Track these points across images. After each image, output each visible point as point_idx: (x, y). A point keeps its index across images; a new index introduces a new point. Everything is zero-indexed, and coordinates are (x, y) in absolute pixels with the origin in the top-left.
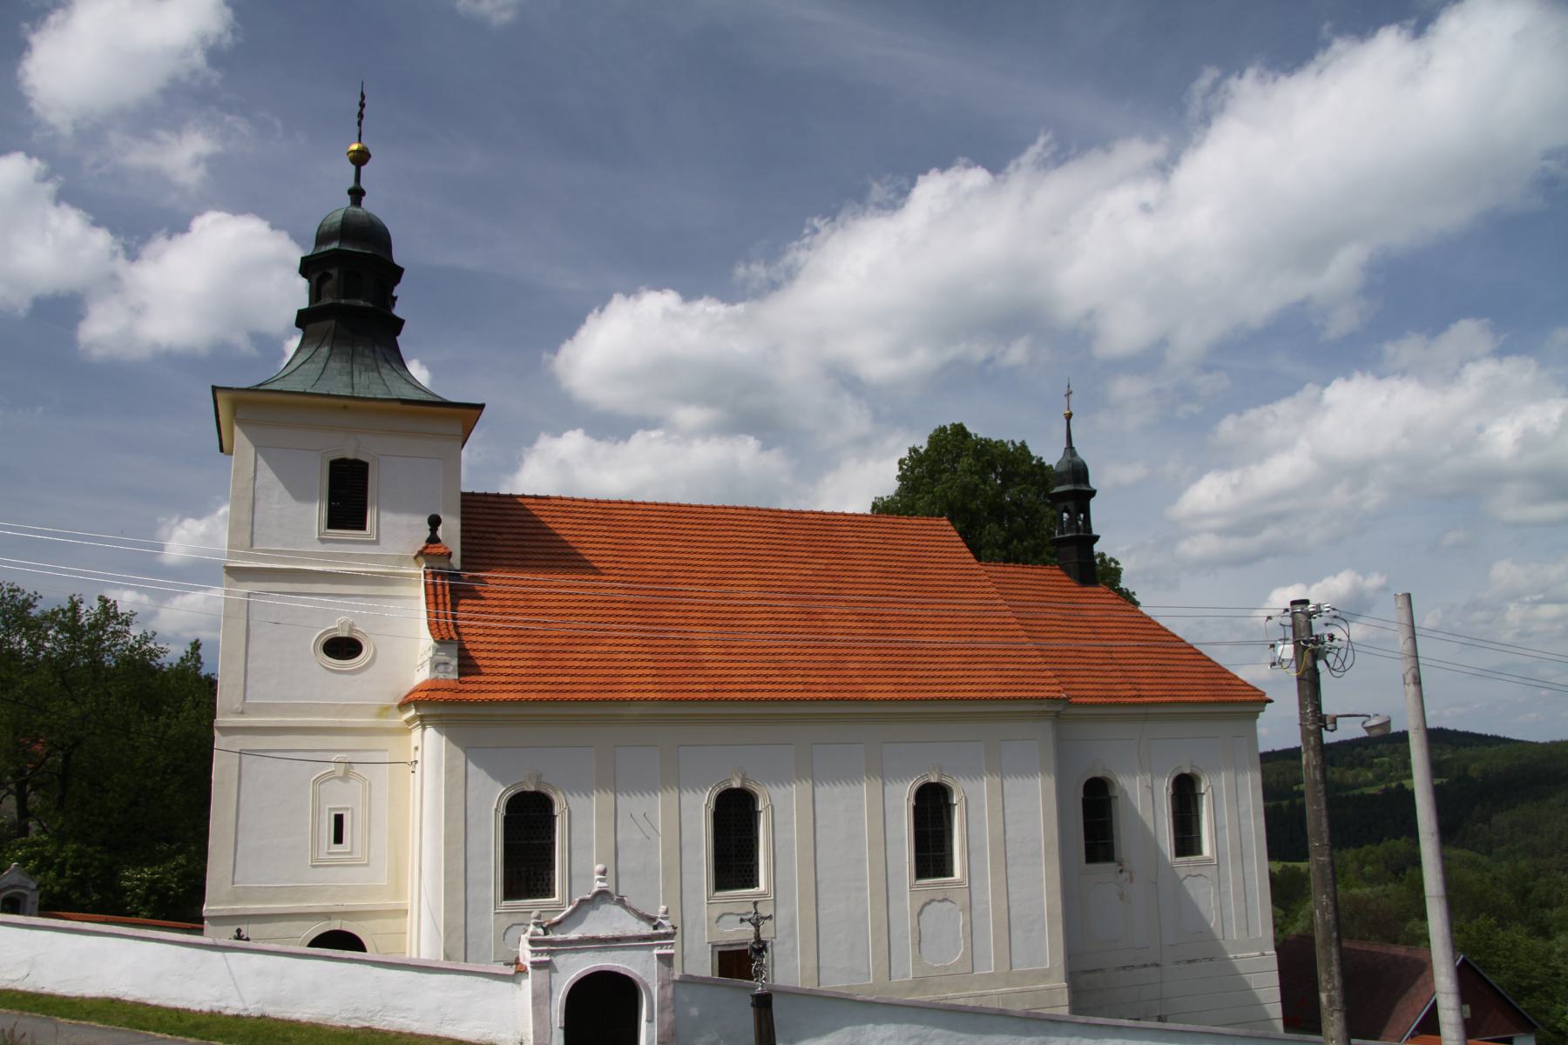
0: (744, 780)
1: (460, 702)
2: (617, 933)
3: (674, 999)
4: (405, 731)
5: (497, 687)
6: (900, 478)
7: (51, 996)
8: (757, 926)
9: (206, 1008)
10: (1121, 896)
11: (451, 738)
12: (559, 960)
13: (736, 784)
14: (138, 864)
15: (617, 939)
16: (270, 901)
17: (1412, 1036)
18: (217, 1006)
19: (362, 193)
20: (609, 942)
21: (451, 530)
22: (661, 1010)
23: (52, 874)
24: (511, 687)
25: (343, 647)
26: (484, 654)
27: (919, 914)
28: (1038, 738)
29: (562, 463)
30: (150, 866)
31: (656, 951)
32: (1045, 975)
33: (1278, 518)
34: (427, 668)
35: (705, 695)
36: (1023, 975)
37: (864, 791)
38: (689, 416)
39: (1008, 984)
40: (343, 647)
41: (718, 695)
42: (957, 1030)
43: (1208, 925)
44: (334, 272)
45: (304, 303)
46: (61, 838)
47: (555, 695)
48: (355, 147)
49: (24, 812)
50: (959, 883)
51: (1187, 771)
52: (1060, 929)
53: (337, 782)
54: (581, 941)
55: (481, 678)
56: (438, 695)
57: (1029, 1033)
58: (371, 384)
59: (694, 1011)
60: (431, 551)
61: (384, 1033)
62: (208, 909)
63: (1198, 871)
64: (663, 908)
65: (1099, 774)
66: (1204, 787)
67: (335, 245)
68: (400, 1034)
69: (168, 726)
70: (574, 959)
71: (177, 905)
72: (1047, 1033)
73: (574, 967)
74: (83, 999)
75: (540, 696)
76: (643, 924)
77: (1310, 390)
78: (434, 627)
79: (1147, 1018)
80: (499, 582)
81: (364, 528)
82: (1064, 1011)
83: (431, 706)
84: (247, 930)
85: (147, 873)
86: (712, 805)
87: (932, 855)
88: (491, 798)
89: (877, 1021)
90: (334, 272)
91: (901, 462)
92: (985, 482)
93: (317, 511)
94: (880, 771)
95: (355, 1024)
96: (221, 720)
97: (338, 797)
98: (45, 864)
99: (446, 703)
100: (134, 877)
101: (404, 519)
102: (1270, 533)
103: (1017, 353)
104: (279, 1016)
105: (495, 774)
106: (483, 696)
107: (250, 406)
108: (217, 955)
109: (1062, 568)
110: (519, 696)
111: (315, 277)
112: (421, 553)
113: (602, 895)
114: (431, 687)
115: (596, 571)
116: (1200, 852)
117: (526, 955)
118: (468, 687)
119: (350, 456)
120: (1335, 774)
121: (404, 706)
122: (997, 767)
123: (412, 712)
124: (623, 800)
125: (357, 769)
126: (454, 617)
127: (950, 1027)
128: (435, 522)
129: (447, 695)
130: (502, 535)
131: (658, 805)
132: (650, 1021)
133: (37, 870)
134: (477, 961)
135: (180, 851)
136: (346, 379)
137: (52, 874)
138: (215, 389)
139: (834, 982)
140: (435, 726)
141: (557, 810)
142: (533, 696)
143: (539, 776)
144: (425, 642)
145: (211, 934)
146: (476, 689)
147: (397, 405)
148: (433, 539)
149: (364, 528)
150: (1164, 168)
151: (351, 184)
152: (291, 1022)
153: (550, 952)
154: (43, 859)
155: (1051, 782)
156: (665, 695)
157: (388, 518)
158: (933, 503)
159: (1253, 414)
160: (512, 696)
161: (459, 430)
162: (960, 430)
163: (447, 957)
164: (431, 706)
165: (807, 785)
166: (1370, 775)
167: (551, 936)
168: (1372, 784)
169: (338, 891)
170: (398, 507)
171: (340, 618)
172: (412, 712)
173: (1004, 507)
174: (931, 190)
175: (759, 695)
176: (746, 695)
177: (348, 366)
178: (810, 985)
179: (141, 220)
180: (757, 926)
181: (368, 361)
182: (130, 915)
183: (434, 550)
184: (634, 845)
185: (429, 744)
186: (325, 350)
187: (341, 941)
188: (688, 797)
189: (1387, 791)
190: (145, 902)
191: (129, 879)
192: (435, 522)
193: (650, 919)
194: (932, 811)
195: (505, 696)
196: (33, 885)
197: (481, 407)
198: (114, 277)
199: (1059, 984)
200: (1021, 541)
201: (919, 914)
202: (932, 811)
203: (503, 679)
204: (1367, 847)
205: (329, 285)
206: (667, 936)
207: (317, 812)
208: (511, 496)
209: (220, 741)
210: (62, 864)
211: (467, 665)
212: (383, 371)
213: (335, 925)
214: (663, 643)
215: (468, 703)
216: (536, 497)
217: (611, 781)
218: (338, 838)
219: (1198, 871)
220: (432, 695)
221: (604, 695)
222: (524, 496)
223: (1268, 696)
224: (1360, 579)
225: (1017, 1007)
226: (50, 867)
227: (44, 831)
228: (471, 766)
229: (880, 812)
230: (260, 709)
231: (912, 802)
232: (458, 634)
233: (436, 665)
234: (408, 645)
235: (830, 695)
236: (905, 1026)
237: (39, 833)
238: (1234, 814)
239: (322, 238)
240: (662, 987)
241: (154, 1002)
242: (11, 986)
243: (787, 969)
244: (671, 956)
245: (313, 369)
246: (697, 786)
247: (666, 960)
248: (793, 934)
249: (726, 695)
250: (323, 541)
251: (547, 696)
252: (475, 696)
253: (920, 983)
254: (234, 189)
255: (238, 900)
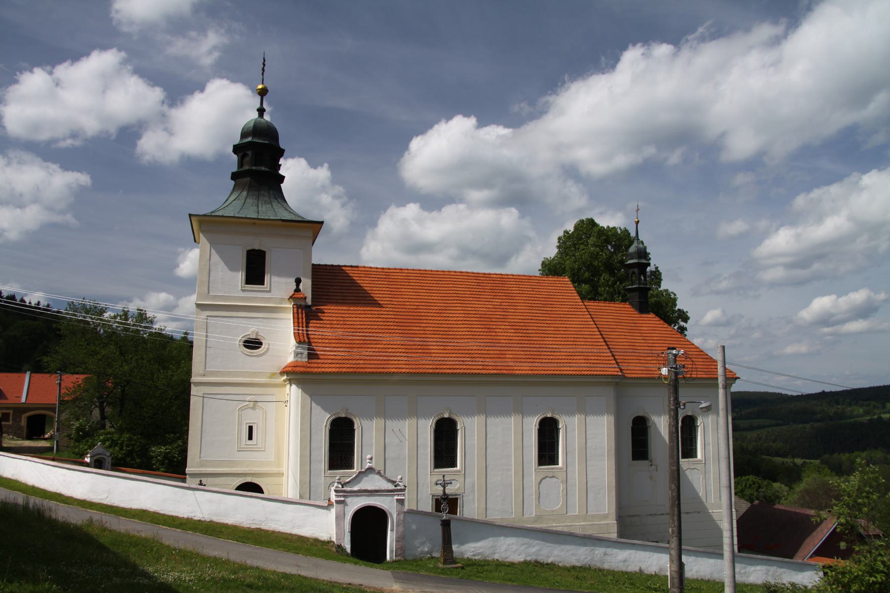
0: (450, 414)
1: (308, 373)
2: (377, 488)
3: (404, 520)
4: (283, 386)
5: (327, 365)
6: (558, 247)
7: (117, 507)
8: (444, 487)
9: (185, 516)
10: (651, 478)
11: (304, 390)
12: (349, 500)
13: (446, 416)
14: (159, 444)
15: (377, 491)
16: (218, 467)
17: (811, 557)
18: (190, 515)
19: (264, 110)
20: (372, 493)
21: (306, 286)
22: (398, 525)
23: (117, 448)
24: (333, 366)
25: (253, 344)
26: (321, 348)
27: (540, 483)
28: (607, 395)
29: (404, 221)
30: (164, 445)
31: (396, 497)
32: (605, 517)
33: (820, 257)
34: (292, 355)
35: (431, 371)
36: (593, 516)
37: (512, 421)
38: (477, 195)
39: (585, 520)
40: (253, 344)
41: (438, 371)
42: (548, 542)
43: (698, 495)
44: (250, 153)
45: (235, 169)
46: (121, 430)
47: (355, 370)
48: (260, 87)
49: (103, 417)
50: (561, 468)
51: (690, 414)
52: (613, 493)
53: (249, 410)
54: (359, 491)
55: (319, 361)
56: (298, 369)
57: (585, 545)
58: (268, 211)
59: (414, 527)
60: (296, 296)
61: (267, 531)
62: (188, 470)
63: (694, 466)
64: (400, 477)
65: (641, 414)
66: (699, 422)
67: (250, 139)
68: (273, 532)
69: (173, 376)
70: (355, 499)
71: (174, 467)
72: (594, 545)
73: (355, 504)
74: (131, 509)
75: (348, 370)
76: (390, 484)
77: (855, 176)
78: (297, 335)
79: (662, 541)
80: (331, 311)
81: (263, 284)
82: (614, 536)
83: (294, 374)
84: (204, 481)
85: (163, 449)
86: (434, 426)
87: (547, 453)
88: (323, 420)
89: (506, 536)
90: (250, 153)
91: (559, 239)
92: (602, 251)
93: (240, 276)
94: (521, 411)
95: (253, 526)
96: (194, 379)
97: (250, 417)
98: (114, 443)
99: (301, 373)
100: (157, 450)
101: (283, 280)
102: (816, 266)
103: (675, 158)
104: (219, 521)
105: (326, 409)
106: (320, 370)
107: (208, 225)
108: (191, 492)
109: (630, 304)
110: (337, 370)
111: (241, 154)
112: (291, 297)
113: (370, 470)
114: (294, 365)
115: (380, 306)
116: (696, 457)
117: (333, 498)
118: (312, 365)
119: (257, 248)
120: (737, 422)
121: (282, 373)
122: (583, 410)
123: (285, 377)
124: (389, 423)
125: (259, 404)
126: (307, 327)
127: (543, 540)
128: (298, 281)
129: (302, 369)
130: (333, 288)
131: (406, 426)
132: (392, 530)
133: (110, 447)
134: (315, 500)
135: (179, 438)
136: (255, 208)
137: (117, 448)
138: (190, 215)
139: (494, 516)
140: (295, 384)
141: (356, 427)
142: (344, 370)
143: (347, 410)
144: (291, 343)
145: (191, 482)
146: (318, 367)
147: (280, 222)
148: (297, 290)
149: (263, 284)
150: (776, 42)
151: (258, 106)
152: (223, 524)
153: (344, 496)
154: (113, 441)
155: (612, 419)
156: (411, 371)
157: (275, 279)
158: (575, 262)
159: (816, 194)
160: (334, 370)
161: (311, 235)
162: (592, 223)
163: (301, 497)
164: (294, 374)
165: (483, 417)
166: (861, 411)
167: (345, 489)
168: (862, 416)
169: (250, 463)
170: (280, 274)
171: (251, 328)
172: (285, 377)
173: (607, 267)
174: (632, 56)
175: (458, 371)
176: (452, 371)
177: (256, 201)
178: (482, 518)
179: (178, 87)
180: (444, 487)
181: (266, 199)
182: (154, 470)
183: (298, 295)
184: (394, 446)
185: (293, 392)
186: (245, 193)
187: (251, 488)
188: (422, 422)
189: (871, 421)
190: (163, 464)
191: (154, 452)
192: (298, 281)
193: (393, 482)
194: (548, 433)
195: (330, 370)
196: (108, 454)
197: (322, 223)
198: (163, 115)
199: (612, 522)
200: (621, 283)
201: (540, 483)
202: (548, 433)
203: (330, 361)
204: (856, 453)
205: (247, 159)
206: (401, 490)
207: (240, 424)
208: (339, 266)
209: (194, 390)
210: (122, 444)
211: (312, 355)
212: (274, 204)
213: (249, 479)
214: (412, 343)
215: (312, 373)
216: (351, 266)
217: (383, 413)
218: (250, 438)
219: (694, 466)
220: (295, 369)
221: (380, 370)
222: (345, 266)
223: (737, 375)
224: (872, 294)
225: (578, 531)
226: (116, 445)
227: (113, 426)
228: (313, 404)
229: (517, 432)
230: (212, 374)
231: (537, 426)
232: (308, 338)
233: (297, 354)
234: (283, 341)
235: (495, 372)
236: (520, 539)
237: (110, 427)
238: (714, 437)
239: (244, 135)
240: (398, 515)
241: (162, 512)
242: (100, 502)
243: (470, 509)
244: (403, 500)
245: (239, 203)
246: (426, 416)
247: (401, 502)
248: (474, 491)
249: (441, 371)
250: (243, 291)
251: (351, 370)
252: (316, 370)
253: (538, 518)
254: (229, 68)
255: (202, 466)
